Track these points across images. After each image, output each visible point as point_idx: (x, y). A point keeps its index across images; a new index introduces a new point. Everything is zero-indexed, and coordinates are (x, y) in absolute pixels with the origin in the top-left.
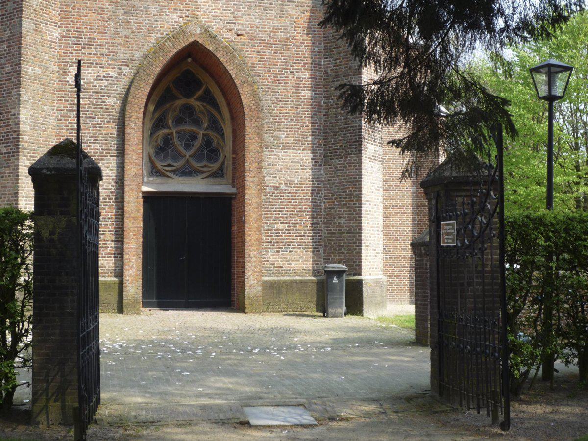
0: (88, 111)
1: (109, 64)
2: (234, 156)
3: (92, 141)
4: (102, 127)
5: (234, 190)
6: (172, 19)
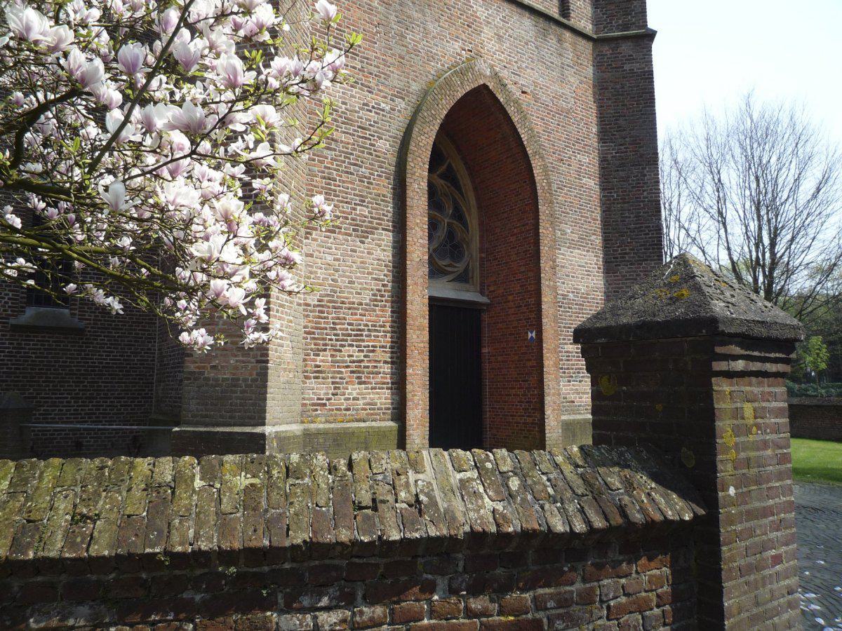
0: (352, 154)
1: (380, 90)
2: (483, 255)
3: (357, 202)
4: (371, 184)
5: (484, 300)
6: (451, 50)
